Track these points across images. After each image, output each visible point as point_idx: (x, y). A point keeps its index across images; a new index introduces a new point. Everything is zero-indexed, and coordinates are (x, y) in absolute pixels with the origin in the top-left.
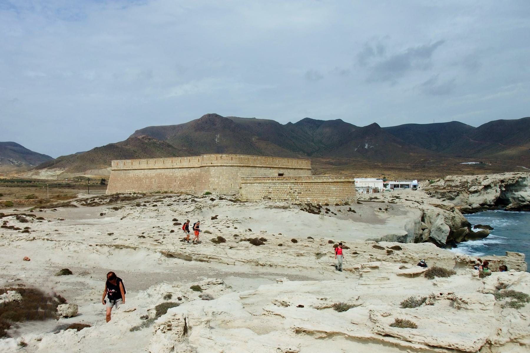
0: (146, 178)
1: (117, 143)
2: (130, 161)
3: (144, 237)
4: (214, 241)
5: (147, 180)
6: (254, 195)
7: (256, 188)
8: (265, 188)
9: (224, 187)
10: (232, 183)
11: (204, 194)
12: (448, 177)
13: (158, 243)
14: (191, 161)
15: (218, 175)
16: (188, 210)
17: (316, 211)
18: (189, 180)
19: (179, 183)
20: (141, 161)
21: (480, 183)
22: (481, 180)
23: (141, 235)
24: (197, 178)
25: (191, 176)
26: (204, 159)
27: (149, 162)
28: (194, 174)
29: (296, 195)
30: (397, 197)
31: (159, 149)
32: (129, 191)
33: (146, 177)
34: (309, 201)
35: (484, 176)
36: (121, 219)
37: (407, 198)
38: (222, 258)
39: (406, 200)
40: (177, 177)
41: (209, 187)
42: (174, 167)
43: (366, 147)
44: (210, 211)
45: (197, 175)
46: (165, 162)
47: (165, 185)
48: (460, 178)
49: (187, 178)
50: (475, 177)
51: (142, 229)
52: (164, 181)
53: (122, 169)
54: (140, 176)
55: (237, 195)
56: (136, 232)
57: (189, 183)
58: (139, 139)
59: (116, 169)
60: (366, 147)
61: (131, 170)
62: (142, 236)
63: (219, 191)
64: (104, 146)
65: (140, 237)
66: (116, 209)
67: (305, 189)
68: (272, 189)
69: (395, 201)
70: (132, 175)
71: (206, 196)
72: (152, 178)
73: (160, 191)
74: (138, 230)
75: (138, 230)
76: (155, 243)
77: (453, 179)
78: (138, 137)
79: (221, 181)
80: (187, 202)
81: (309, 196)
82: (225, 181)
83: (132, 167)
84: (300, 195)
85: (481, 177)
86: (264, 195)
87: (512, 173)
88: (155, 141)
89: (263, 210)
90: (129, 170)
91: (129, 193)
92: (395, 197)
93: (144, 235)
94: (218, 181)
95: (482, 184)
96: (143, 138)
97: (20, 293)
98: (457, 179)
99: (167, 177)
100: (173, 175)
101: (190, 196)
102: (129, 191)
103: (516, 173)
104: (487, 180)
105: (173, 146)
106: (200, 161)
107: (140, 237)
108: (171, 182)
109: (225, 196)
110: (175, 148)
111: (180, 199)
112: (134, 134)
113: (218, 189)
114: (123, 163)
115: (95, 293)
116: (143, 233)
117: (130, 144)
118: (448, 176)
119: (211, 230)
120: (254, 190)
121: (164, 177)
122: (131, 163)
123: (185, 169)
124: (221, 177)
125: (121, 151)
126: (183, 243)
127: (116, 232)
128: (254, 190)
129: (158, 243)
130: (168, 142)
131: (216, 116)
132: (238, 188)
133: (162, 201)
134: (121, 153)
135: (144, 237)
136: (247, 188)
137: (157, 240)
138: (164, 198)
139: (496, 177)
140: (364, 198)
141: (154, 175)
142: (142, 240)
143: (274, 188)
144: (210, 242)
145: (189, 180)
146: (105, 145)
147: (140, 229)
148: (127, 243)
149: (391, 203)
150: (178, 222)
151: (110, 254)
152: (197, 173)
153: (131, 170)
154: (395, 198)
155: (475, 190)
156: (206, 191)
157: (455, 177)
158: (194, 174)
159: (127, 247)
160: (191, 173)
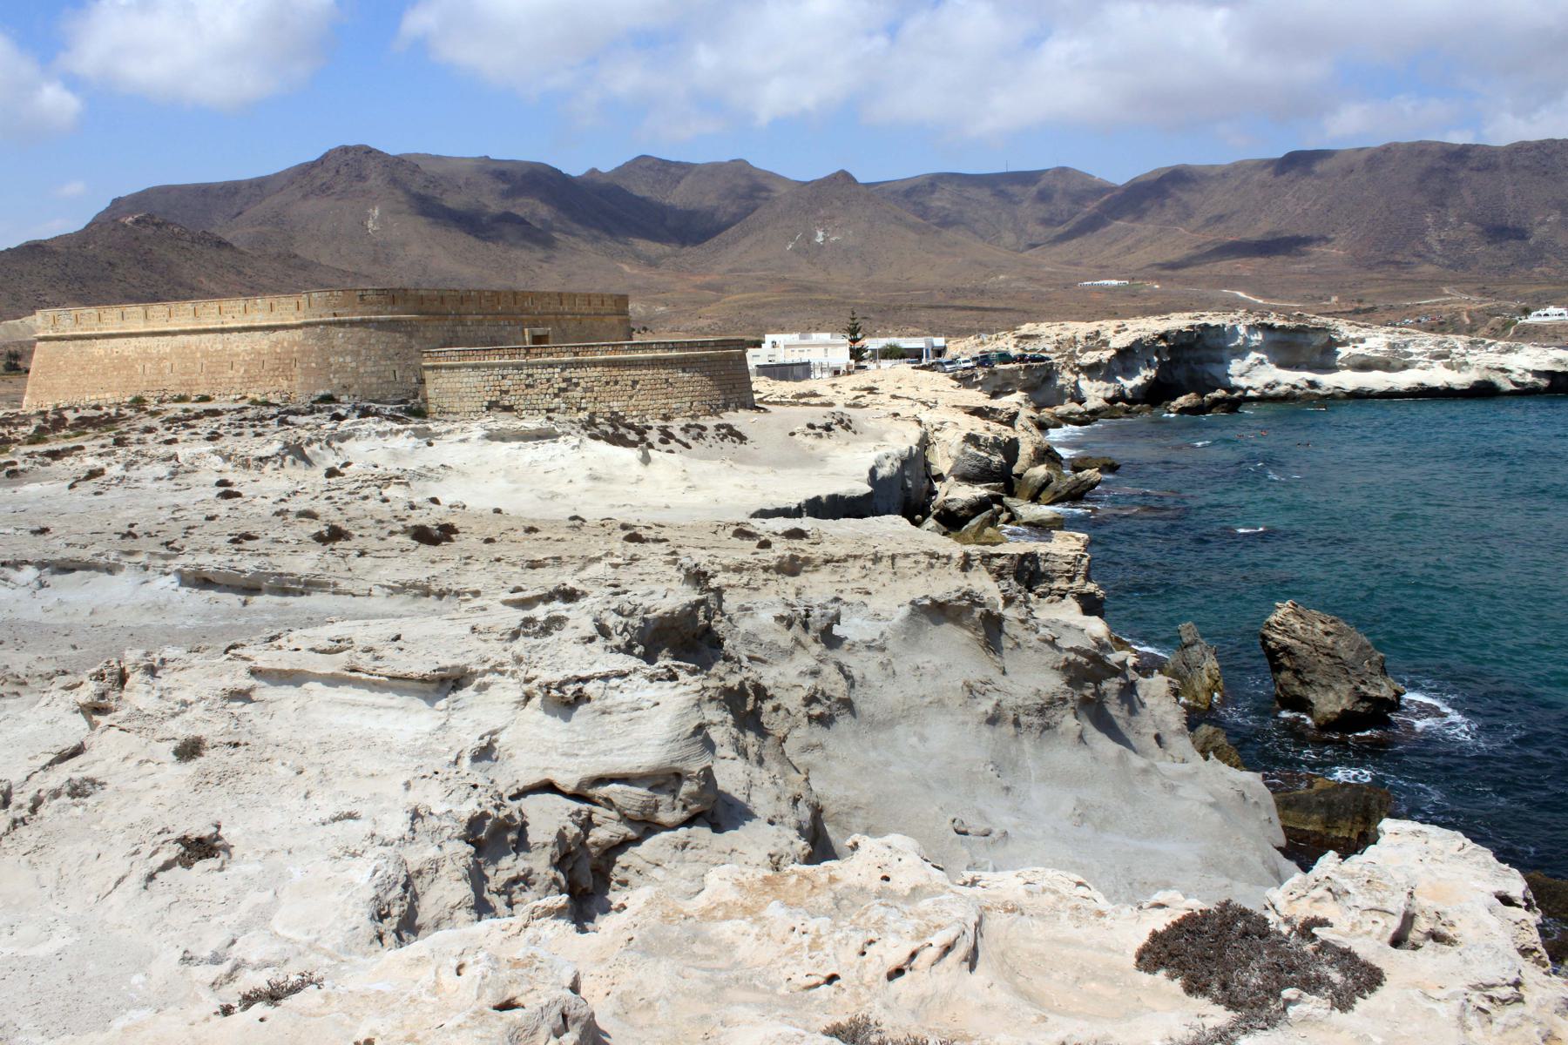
0: (145, 359)
1: (51, 240)
2: (93, 310)
3: (135, 537)
4: (319, 538)
5: (148, 365)
6: (461, 399)
7: (465, 380)
8: (491, 378)
9: (374, 380)
10: (396, 368)
11: (314, 402)
12: (1026, 329)
13: (173, 549)
14: (276, 308)
15: (355, 348)
16: (263, 453)
17: (633, 436)
18: (273, 361)
19: (242, 371)
20: (128, 310)
21: (1106, 343)
22: (1110, 333)
23: (125, 530)
24: (295, 355)
25: (278, 350)
26: (312, 302)
27: (150, 313)
28: (285, 344)
29: (580, 395)
30: (871, 390)
31: (188, 255)
32: (93, 397)
33: (146, 356)
34: (616, 410)
35: (1118, 322)
36: (72, 487)
37: (898, 393)
38: (338, 581)
39: (894, 397)
40: (238, 355)
41: (330, 380)
42: (226, 326)
43: (820, 240)
44: (329, 454)
45: (295, 349)
46: (198, 314)
47: (202, 379)
48: (1056, 328)
49: (265, 358)
50: (1093, 326)
51: (131, 513)
52: (199, 366)
53: (69, 333)
54: (126, 354)
55: (412, 401)
56: (112, 521)
57: (274, 370)
58: (125, 226)
59: (51, 333)
60: (820, 240)
61: (97, 337)
62: (130, 534)
63: (359, 393)
64: (9, 250)
65: (124, 536)
66: (55, 455)
67: (604, 379)
68: (510, 383)
69: (863, 401)
70: (102, 352)
71: (321, 406)
72: (162, 359)
73: (188, 394)
74: (119, 516)
75: (119, 516)
76: (164, 551)
77: (1037, 332)
78: (122, 220)
79: (364, 364)
80: (263, 426)
81: (617, 398)
82: (376, 363)
83: (100, 329)
84: (588, 394)
85: (1108, 327)
86: (488, 399)
87: (1187, 315)
88: (176, 230)
89: (480, 442)
90: (89, 338)
91: (94, 403)
92: (865, 389)
93: (133, 530)
94: (354, 365)
95: (1111, 345)
96: (137, 222)
97: (942, 604)
98: (1048, 332)
99: (206, 354)
100: (224, 349)
101: (274, 411)
102: (93, 397)
103: (1197, 314)
104: (1123, 334)
105: (235, 244)
106: (302, 307)
107: (124, 536)
108: (219, 369)
109: (377, 406)
110: (242, 253)
111: (245, 419)
112: (108, 210)
113: (356, 386)
114: (73, 317)
115: (187, 959)
116: (132, 526)
117: (95, 243)
118: (1028, 325)
119: (321, 506)
120: (458, 385)
121: (199, 355)
122: (96, 318)
123: (258, 334)
124: (363, 352)
125: (66, 265)
126: (237, 546)
127: (57, 525)
128: (458, 385)
129: (173, 549)
130: (219, 234)
131: (369, 151)
132: (414, 380)
133: (194, 427)
134: (68, 271)
135: (135, 537)
136: (440, 380)
137: (167, 544)
138: (198, 416)
139: (1147, 327)
140: (779, 393)
141: (168, 350)
142: (129, 544)
143: (517, 377)
144: (310, 539)
145: (273, 361)
146: (13, 246)
147: (125, 514)
148: (87, 555)
149: (855, 406)
150: (235, 489)
151: (42, 585)
152: (295, 343)
153: (97, 337)
154: (865, 393)
155: (1093, 361)
156: (322, 392)
157: (1042, 328)
158: (285, 344)
159: (87, 566)
160: (277, 343)
